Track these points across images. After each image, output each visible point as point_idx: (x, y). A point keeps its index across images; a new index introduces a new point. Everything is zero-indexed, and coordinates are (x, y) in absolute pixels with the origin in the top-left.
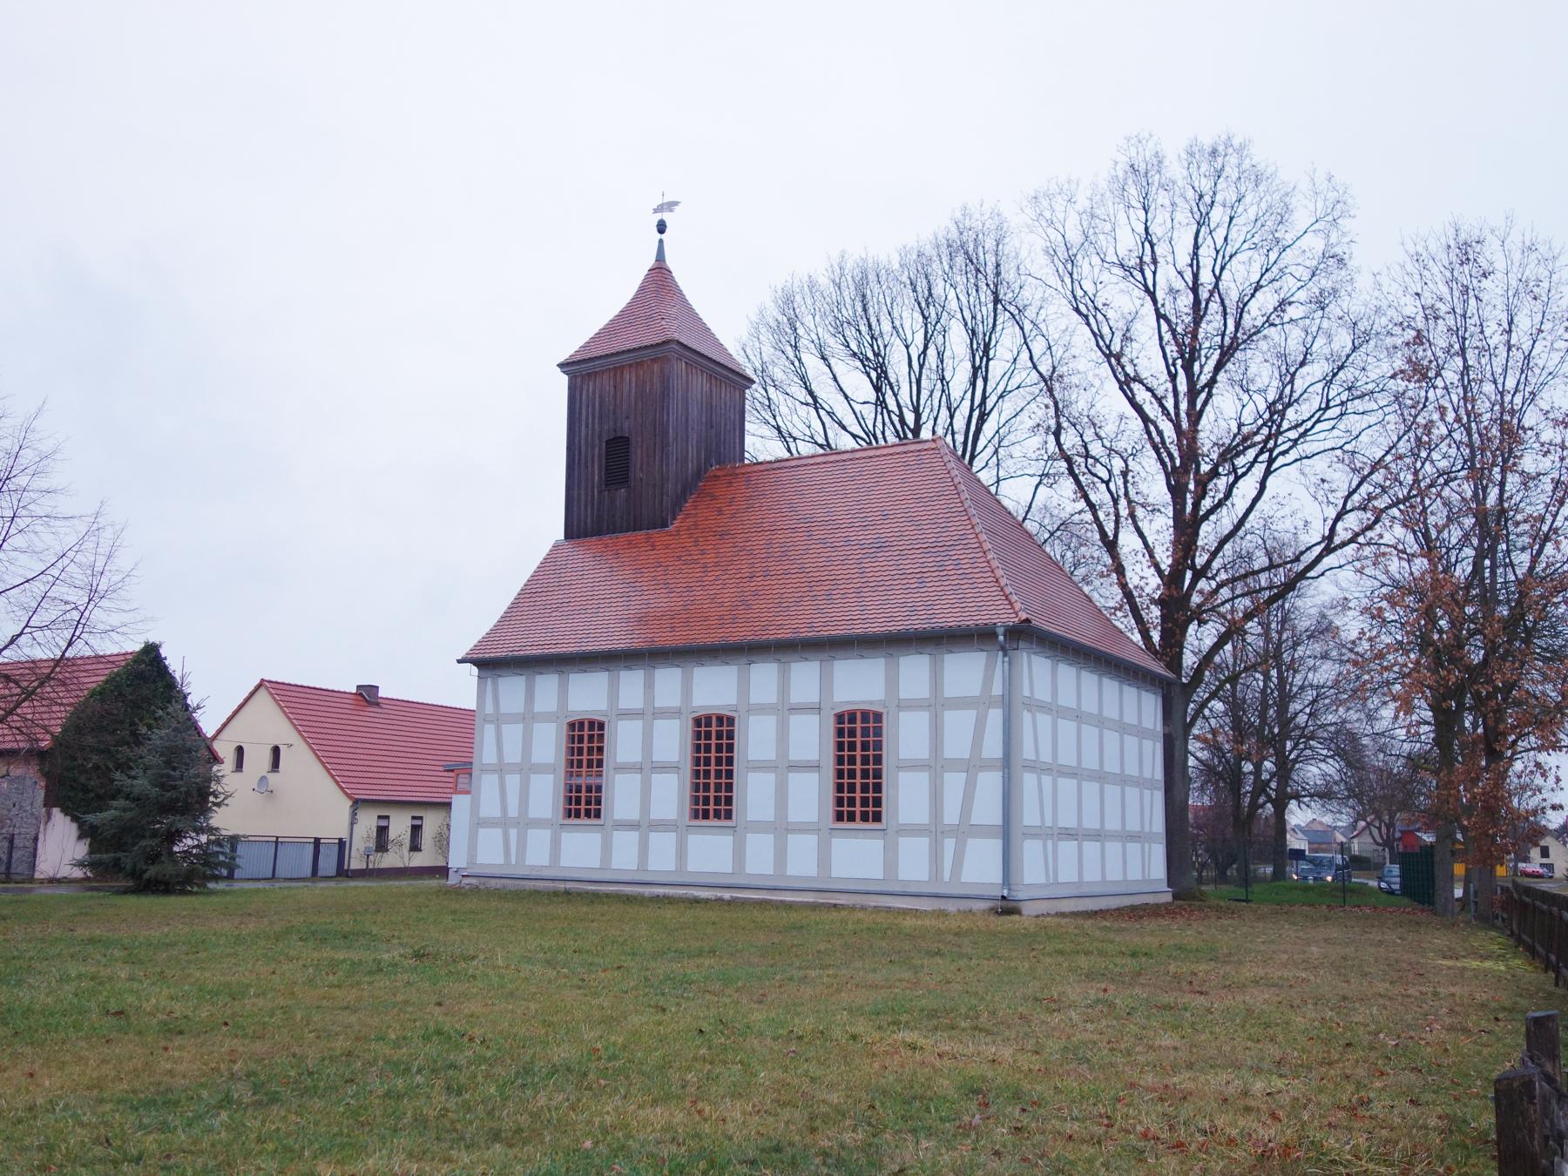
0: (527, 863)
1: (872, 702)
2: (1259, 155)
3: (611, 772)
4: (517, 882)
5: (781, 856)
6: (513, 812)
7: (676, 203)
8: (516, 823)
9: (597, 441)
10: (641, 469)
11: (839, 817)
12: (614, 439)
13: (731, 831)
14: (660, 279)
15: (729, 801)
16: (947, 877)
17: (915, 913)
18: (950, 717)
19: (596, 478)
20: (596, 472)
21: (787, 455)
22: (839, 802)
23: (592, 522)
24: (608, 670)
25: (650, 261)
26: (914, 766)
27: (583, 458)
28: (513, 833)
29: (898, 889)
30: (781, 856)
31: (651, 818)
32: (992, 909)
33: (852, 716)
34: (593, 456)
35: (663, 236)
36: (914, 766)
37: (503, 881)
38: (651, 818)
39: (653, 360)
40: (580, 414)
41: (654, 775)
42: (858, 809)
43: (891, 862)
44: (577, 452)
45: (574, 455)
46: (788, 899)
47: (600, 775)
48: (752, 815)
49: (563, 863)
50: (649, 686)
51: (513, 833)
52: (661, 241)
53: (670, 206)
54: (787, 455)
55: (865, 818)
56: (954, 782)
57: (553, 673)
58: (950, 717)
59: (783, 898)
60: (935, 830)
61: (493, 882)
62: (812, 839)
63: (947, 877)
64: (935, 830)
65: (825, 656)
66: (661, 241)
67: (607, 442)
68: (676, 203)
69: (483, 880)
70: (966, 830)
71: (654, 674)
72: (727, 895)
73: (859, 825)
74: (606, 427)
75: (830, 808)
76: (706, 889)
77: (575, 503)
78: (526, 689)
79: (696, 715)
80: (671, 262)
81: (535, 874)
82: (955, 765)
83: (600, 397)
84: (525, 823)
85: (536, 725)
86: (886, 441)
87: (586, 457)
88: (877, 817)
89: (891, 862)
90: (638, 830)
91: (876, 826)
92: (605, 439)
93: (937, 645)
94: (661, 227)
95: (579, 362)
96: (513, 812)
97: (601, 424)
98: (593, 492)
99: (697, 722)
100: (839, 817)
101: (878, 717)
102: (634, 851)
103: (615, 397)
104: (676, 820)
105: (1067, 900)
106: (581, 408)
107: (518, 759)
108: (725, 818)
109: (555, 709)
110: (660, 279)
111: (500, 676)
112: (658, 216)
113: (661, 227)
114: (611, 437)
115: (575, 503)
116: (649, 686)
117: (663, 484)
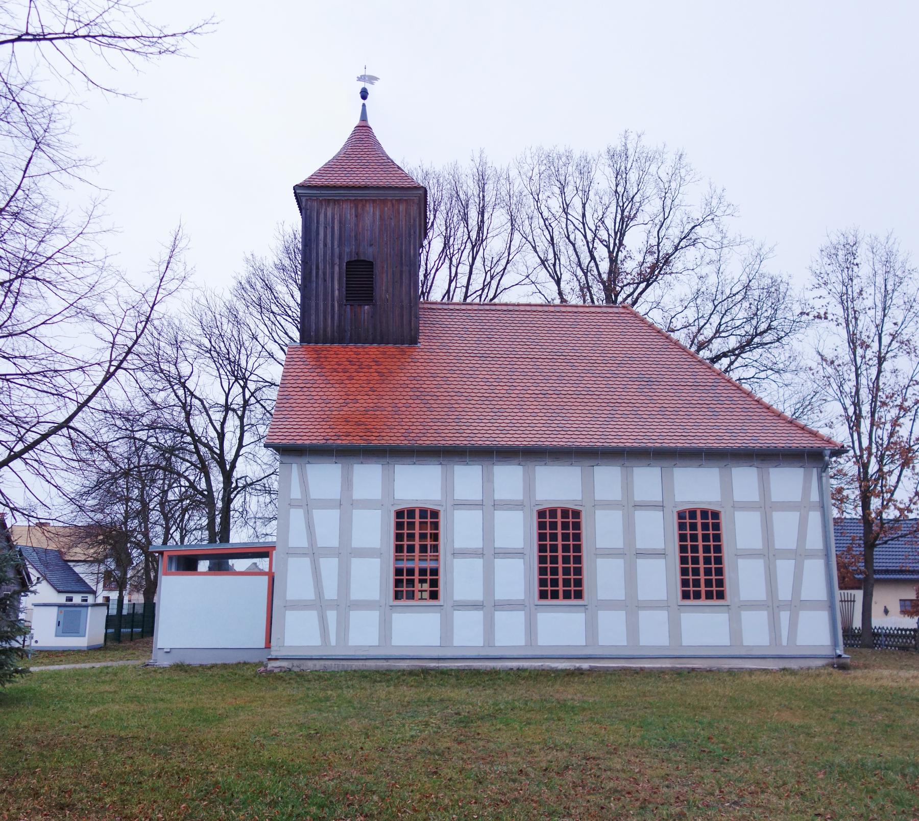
0: (350, 644)
1: (710, 503)
2: (650, 143)
3: (449, 556)
4: (338, 662)
5: (633, 629)
6: (331, 592)
7: (376, 79)
8: (335, 605)
9: (337, 261)
10: (387, 291)
11: (543, 595)
12: (355, 261)
13: (583, 608)
14: (363, 131)
15: (720, 583)
16: (784, 642)
17: (766, 672)
18: (778, 517)
19: (337, 293)
20: (336, 286)
21: (581, 303)
22: (685, 583)
23: (333, 332)
24: (441, 464)
25: (356, 121)
26: (751, 554)
27: (321, 273)
28: (332, 616)
29: (743, 653)
30: (633, 629)
31: (496, 598)
32: (828, 665)
33: (693, 513)
34: (333, 273)
35: (366, 102)
36: (751, 554)
37: (322, 662)
38: (496, 598)
39: (399, 201)
40: (318, 234)
41: (496, 560)
42: (703, 589)
43: (736, 631)
44: (314, 267)
45: (311, 272)
46: (646, 666)
47: (437, 559)
48: (602, 595)
49: (395, 642)
50: (488, 480)
51: (332, 616)
52: (364, 105)
53: (372, 79)
54: (581, 303)
55: (709, 596)
56: (785, 568)
57: (377, 463)
58: (778, 517)
59: (642, 666)
60: (772, 605)
61: (310, 664)
62: (662, 615)
63: (784, 642)
64: (772, 605)
65: (665, 463)
66: (364, 105)
67: (348, 263)
68: (376, 79)
69: (296, 663)
70: (797, 605)
71: (352, 468)
72: (585, 665)
73: (703, 602)
74: (347, 250)
75: (536, 589)
76: (563, 660)
77: (313, 312)
78: (342, 476)
79: (540, 508)
80: (371, 122)
81: (360, 653)
82: (785, 554)
83: (340, 222)
84: (797, 605)
85: (794, 546)
86: (593, 301)
87: (324, 274)
88: (721, 595)
89: (736, 631)
90: (482, 609)
91: (720, 602)
92: (346, 260)
93: (762, 460)
94: (364, 94)
95: (309, 187)
96: (331, 592)
97: (340, 245)
98: (333, 306)
99: (681, 515)
100: (543, 595)
101: (435, 514)
102: (479, 629)
103: (357, 225)
104: (523, 600)
105: (716, 660)
106: (318, 227)
107: (335, 543)
108: (717, 598)
109: (379, 497)
110: (363, 131)
111: (309, 463)
112: (362, 85)
113: (364, 94)
114: (353, 259)
115: (313, 312)
116: (488, 480)
117: (411, 307)
